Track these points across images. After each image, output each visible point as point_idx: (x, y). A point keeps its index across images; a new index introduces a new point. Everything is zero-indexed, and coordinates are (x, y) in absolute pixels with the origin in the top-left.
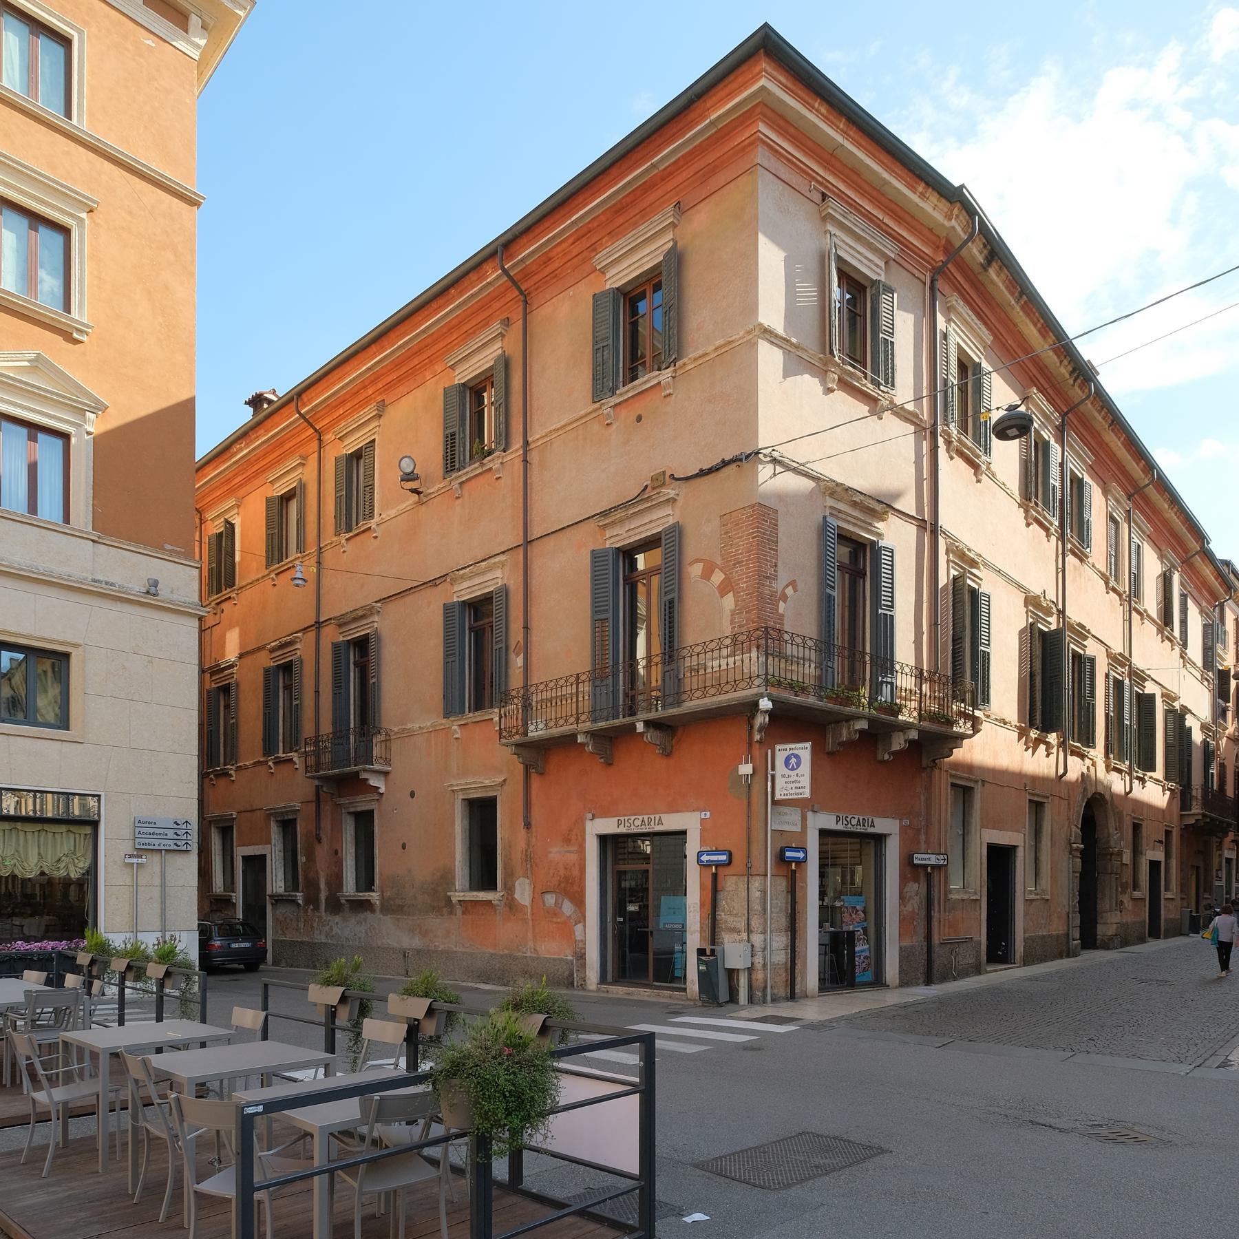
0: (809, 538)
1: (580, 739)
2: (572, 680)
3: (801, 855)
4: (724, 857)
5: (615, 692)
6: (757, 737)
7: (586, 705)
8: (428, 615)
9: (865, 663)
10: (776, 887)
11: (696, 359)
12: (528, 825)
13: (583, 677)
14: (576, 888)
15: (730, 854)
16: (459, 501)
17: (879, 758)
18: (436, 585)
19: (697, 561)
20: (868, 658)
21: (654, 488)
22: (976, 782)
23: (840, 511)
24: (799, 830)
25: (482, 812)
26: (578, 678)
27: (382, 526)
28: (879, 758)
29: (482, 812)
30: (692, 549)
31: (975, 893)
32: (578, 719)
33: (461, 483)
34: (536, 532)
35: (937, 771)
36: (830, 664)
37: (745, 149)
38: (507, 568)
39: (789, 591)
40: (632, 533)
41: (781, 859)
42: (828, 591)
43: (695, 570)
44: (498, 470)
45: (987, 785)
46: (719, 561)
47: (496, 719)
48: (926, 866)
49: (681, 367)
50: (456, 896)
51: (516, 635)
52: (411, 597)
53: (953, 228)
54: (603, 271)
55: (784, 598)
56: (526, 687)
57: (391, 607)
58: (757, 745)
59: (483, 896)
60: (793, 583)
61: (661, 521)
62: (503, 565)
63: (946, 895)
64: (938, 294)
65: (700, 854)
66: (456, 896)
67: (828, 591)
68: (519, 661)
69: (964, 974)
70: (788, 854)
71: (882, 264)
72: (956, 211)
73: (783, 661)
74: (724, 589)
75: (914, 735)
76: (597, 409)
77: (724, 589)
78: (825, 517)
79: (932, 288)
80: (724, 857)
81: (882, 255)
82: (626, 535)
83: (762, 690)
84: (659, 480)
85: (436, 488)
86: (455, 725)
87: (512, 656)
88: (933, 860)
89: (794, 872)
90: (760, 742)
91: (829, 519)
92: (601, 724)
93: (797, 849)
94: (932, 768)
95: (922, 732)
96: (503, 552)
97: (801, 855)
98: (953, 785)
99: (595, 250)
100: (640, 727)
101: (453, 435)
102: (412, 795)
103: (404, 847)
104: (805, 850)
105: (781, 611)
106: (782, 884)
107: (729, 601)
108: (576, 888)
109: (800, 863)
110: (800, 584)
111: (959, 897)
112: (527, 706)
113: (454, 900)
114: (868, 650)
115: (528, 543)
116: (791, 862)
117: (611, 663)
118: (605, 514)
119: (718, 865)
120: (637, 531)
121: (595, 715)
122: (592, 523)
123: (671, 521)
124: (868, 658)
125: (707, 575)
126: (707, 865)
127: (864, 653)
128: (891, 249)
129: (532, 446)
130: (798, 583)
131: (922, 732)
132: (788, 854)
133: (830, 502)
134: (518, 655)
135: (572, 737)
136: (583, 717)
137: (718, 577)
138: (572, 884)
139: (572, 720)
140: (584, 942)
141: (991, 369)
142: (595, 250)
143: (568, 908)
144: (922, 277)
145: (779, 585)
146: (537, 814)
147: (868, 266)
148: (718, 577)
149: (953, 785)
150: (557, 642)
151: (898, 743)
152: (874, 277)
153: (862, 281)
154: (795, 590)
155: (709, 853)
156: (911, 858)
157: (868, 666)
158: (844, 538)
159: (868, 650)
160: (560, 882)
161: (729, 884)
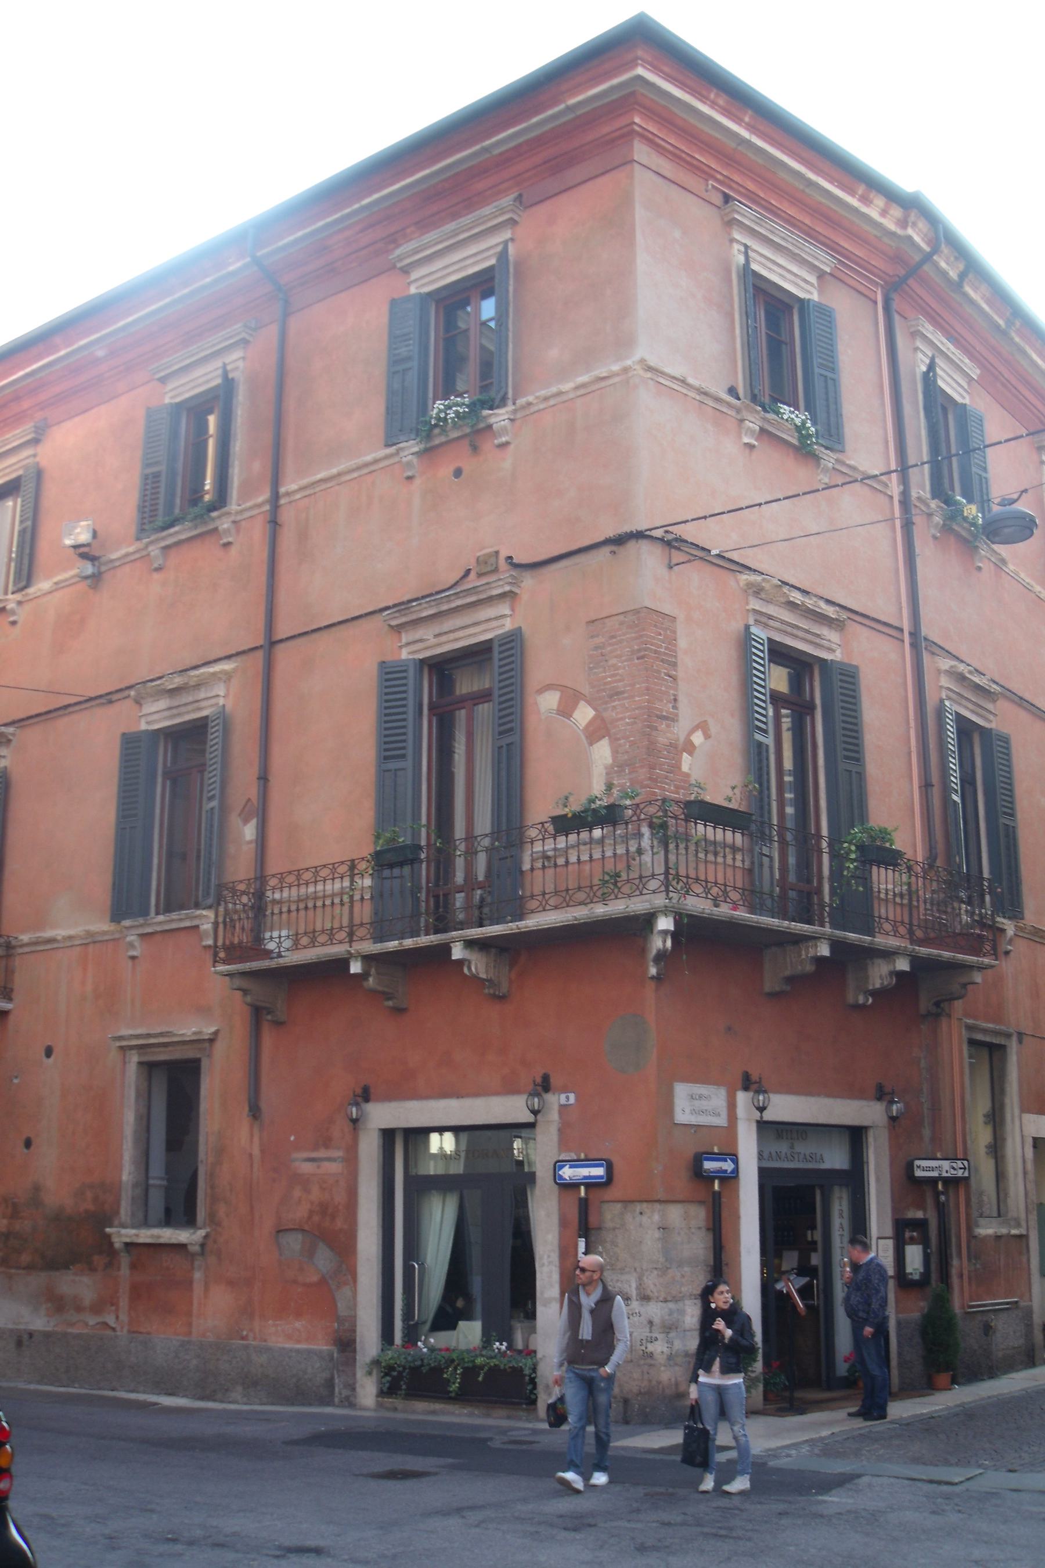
0: (724, 659)
1: (355, 968)
2: (343, 869)
3: (728, 1166)
4: (599, 1171)
5: (416, 889)
6: (653, 971)
7: (364, 912)
8: (93, 750)
9: (820, 851)
10: (686, 1222)
11: (546, 399)
12: (255, 1112)
13: (363, 865)
14: (339, 1224)
15: (610, 1168)
16: (156, 576)
17: (850, 999)
18: (110, 702)
19: (549, 687)
20: (824, 844)
21: (480, 575)
22: (1009, 1036)
23: (770, 617)
24: (722, 1121)
25: (175, 1080)
26: (353, 866)
27: (27, 607)
28: (850, 999)
29: (175, 1080)
30: (540, 668)
31: (1018, 1225)
32: (351, 934)
33: (167, 548)
34: (283, 630)
35: (944, 1022)
36: (765, 851)
37: (628, 135)
38: (235, 682)
39: (698, 738)
40: (444, 638)
41: (699, 1175)
42: (758, 737)
43: (549, 702)
44: (227, 531)
45: (1026, 1039)
46: (586, 690)
47: (207, 927)
48: (933, 1181)
49: (523, 408)
50: (122, 1234)
51: (243, 784)
52: (65, 720)
53: (910, 238)
54: (406, 271)
55: (690, 748)
56: (261, 878)
57: (33, 735)
58: (651, 986)
59: (168, 1235)
60: (703, 726)
61: (494, 624)
62: (228, 676)
63: (969, 1229)
64: (897, 318)
65: (558, 1165)
66: (122, 1234)
67: (758, 737)
68: (249, 832)
69: (1009, 1365)
70: (708, 1165)
71: (813, 279)
72: (912, 218)
73: (703, 878)
74: (596, 731)
75: (903, 965)
76: (390, 456)
77: (596, 731)
78: (747, 627)
79: (887, 308)
80: (599, 1171)
81: (813, 268)
82: (433, 641)
83: (660, 901)
84: (487, 565)
85: (123, 551)
86: (131, 932)
87: (234, 819)
88: (945, 1168)
89: (717, 1197)
90: (657, 979)
91: (754, 630)
92: (392, 945)
93: (721, 1157)
94: (937, 1016)
95: (916, 961)
96: (228, 657)
97: (728, 1166)
98: (972, 1042)
99: (395, 241)
100: (458, 952)
101: (157, 476)
102: (49, 1052)
103: (28, 1144)
104: (735, 1158)
105: (685, 768)
106: (699, 1214)
107: (602, 753)
108: (339, 1224)
109: (730, 1179)
110: (713, 729)
111: (990, 1231)
112: (259, 908)
113: (118, 1243)
114: (825, 832)
115: (272, 644)
116: (711, 1180)
117: (412, 864)
118: (402, 606)
119: (591, 1185)
120: (452, 636)
121: (380, 931)
122: (378, 620)
123: (508, 625)
124: (824, 844)
125: (566, 710)
126: (568, 1187)
127: (819, 836)
128: (826, 262)
129: (282, 501)
130: (711, 722)
131: (916, 961)
132: (708, 1165)
133: (755, 604)
134: (246, 821)
135: (343, 963)
136: (361, 932)
137: (584, 714)
138: (333, 1218)
139: (342, 935)
140: (353, 1319)
141: (740, 148)
142: (395, 241)
143: (324, 1259)
144: (872, 296)
145: (680, 730)
146: (271, 1096)
147: (793, 279)
148: (584, 714)
149: (972, 1042)
150: (321, 811)
151: (879, 975)
152: (802, 295)
153: (786, 300)
154: (707, 736)
155: (575, 1163)
156: (910, 1167)
157: (826, 858)
158: (779, 654)
159: (825, 832)
160: (311, 1213)
161: (608, 1216)
